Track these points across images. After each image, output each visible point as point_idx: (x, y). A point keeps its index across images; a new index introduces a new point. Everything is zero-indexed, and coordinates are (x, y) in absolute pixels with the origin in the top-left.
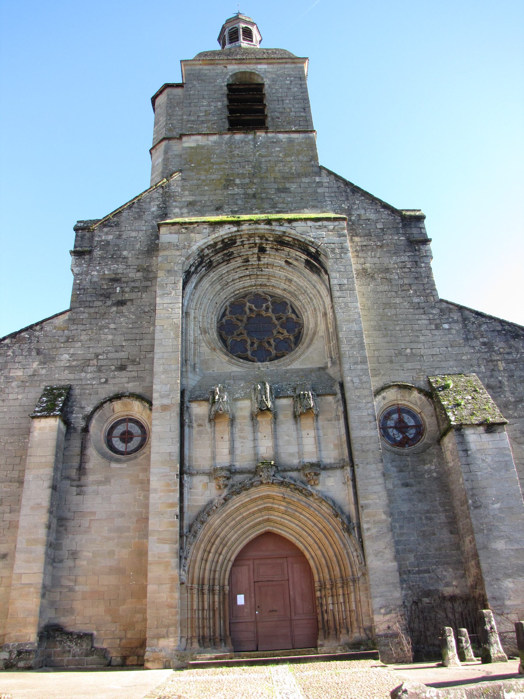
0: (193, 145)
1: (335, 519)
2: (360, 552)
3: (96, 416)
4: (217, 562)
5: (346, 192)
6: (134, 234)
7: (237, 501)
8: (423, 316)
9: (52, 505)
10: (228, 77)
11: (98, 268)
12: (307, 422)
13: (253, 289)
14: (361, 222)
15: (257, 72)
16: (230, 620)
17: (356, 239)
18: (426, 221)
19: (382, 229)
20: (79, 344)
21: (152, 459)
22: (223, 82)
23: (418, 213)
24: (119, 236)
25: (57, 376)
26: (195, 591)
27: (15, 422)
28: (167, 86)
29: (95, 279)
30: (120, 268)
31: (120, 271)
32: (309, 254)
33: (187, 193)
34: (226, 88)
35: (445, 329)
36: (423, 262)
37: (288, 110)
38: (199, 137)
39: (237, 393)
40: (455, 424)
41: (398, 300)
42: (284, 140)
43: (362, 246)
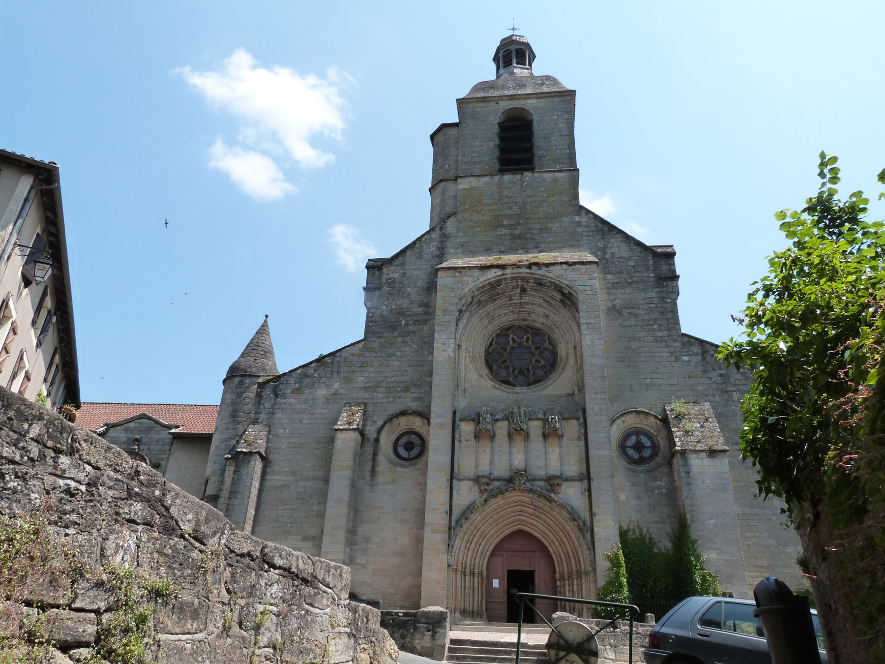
0: (466, 186)
1: (573, 522)
2: (592, 551)
3: (386, 428)
4: (478, 551)
5: (602, 230)
6: (416, 273)
7: (494, 503)
8: (665, 349)
9: (350, 500)
10: (499, 114)
11: (386, 303)
12: (553, 441)
13: (517, 323)
14: (615, 260)
15: (526, 108)
16: (486, 599)
17: (609, 277)
18: (676, 258)
19: (634, 266)
20: (372, 369)
21: (429, 466)
22: (495, 120)
23: (669, 250)
24: (404, 274)
25: (354, 395)
26: (459, 573)
27: (321, 432)
28: (444, 126)
29: (384, 313)
30: (405, 303)
31: (404, 306)
32: (563, 294)
33: (461, 234)
34: (497, 126)
35: (685, 361)
36: (670, 298)
37: (554, 148)
38: (472, 179)
39: (498, 414)
40: (680, 449)
41: (642, 335)
42: (549, 179)
43: (613, 283)
